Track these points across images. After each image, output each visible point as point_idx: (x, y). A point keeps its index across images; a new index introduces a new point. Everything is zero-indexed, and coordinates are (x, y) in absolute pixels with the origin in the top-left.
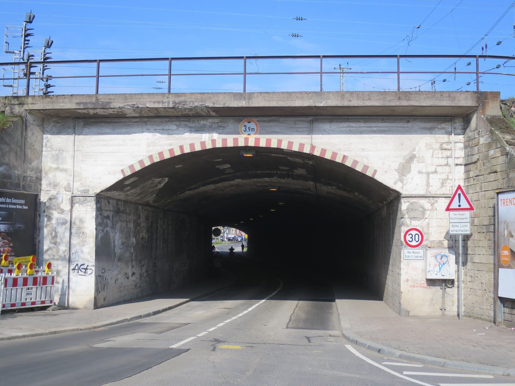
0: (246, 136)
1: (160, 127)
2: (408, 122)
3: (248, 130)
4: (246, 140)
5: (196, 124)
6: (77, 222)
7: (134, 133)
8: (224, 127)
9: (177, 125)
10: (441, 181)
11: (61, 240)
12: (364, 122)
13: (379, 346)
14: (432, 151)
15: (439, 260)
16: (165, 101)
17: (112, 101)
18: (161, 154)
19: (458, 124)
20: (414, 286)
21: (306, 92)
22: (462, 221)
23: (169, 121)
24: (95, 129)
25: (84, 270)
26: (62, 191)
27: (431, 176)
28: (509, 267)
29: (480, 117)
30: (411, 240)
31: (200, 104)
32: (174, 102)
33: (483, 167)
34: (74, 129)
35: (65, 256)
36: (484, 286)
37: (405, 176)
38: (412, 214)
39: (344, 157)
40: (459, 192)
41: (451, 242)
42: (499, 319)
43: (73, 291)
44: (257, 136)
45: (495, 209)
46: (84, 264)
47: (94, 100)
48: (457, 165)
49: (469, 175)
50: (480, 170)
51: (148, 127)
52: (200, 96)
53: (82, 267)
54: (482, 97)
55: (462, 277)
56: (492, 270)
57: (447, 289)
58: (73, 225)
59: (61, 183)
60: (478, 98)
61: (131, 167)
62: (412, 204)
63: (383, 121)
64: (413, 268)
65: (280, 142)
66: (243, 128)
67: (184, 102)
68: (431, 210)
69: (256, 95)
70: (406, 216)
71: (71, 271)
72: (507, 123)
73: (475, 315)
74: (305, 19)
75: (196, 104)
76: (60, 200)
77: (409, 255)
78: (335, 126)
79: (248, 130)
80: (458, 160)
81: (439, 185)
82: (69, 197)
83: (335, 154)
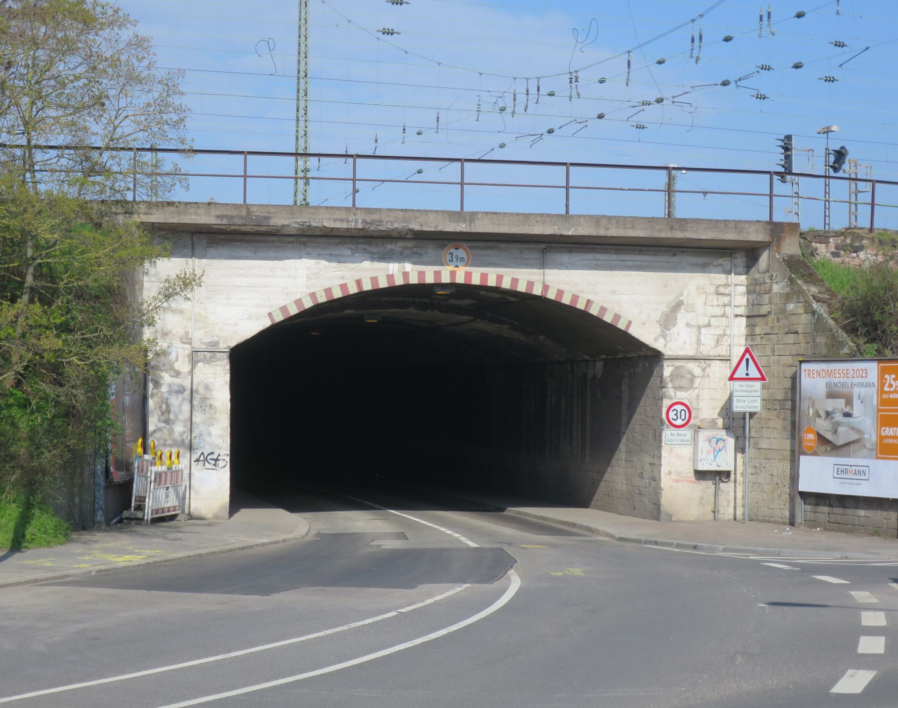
0: (452, 268)
1: (327, 252)
2: (674, 255)
3: (454, 260)
4: (453, 274)
5: (381, 249)
6: (201, 390)
7: (287, 258)
8: (421, 254)
9: (352, 250)
10: (716, 337)
11: (177, 417)
12: (615, 254)
13: (695, 544)
14: (704, 296)
15: (714, 446)
16: (350, 219)
17: (272, 215)
18: (328, 291)
19: (740, 260)
20: (677, 481)
21: (549, 215)
22: (750, 394)
23: (340, 243)
24: (225, 251)
25: (213, 462)
26: (177, 343)
27: (703, 330)
28: (815, 454)
29: (774, 257)
30: (675, 417)
31: (402, 225)
32: (364, 221)
33: (776, 324)
34: (193, 249)
35: (183, 440)
36: (775, 478)
37: (669, 330)
38: (678, 383)
39: (589, 302)
40: (747, 356)
41: (727, 420)
42: (799, 519)
43: (197, 493)
44: (469, 269)
45: (795, 380)
46: (212, 453)
47: (244, 212)
48: (737, 316)
49: (753, 330)
50: (772, 328)
51: (309, 250)
52: (401, 213)
53: (210, 457)
54: (777, 230)
55: (740, 469)
56: (789, 458)
57: (722, 485)
58: (194, 395)
59: (174, 331)
60: (772, 231)
61: (284, 309)
62: (677, 368)
63: (641, 252)
64: (688, 459)
65: (500, 278)
66: (449, 257)
67: (378, 221)
68: (702, 377)
69: (480, 216)
70: (670, 385)
71: (193, 463)
72: (809, 268)
73: (761, 518)
74: (407, 3)
75: (396, 225)
76: (173, 356)
77: (673, 438)
78: (576, 257)
79: (454, 260)
80: (739, 309)
81: (713, 343)
82: (188, 352)
83: (575, 298)
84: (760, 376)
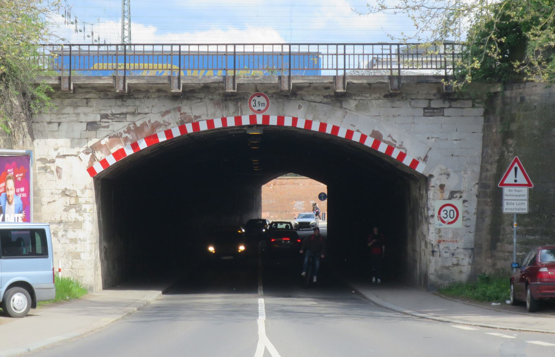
3: (257, 105)
22: (518, 198)
30: (445, 216)
40: (516, 165)
79: (257, 105)
84: (527, 183)
